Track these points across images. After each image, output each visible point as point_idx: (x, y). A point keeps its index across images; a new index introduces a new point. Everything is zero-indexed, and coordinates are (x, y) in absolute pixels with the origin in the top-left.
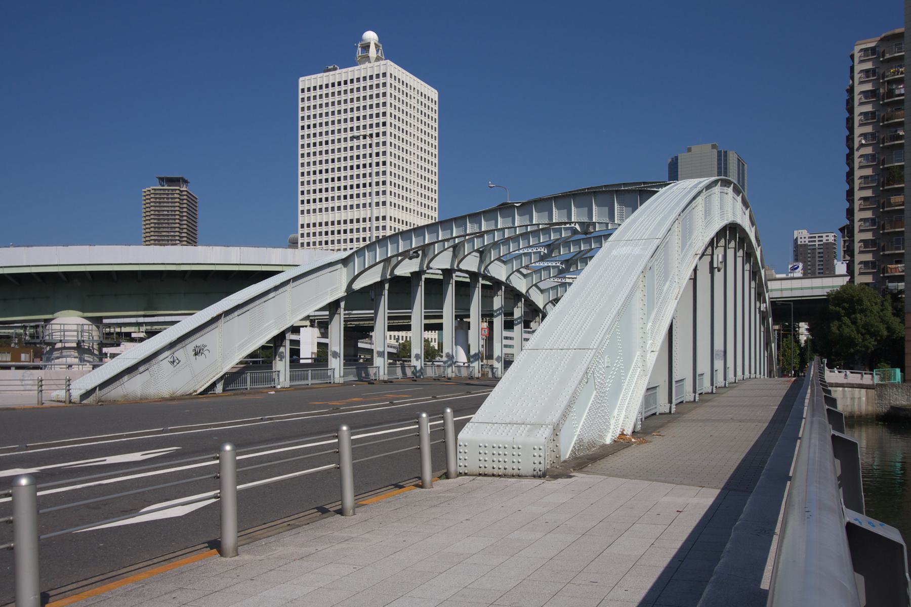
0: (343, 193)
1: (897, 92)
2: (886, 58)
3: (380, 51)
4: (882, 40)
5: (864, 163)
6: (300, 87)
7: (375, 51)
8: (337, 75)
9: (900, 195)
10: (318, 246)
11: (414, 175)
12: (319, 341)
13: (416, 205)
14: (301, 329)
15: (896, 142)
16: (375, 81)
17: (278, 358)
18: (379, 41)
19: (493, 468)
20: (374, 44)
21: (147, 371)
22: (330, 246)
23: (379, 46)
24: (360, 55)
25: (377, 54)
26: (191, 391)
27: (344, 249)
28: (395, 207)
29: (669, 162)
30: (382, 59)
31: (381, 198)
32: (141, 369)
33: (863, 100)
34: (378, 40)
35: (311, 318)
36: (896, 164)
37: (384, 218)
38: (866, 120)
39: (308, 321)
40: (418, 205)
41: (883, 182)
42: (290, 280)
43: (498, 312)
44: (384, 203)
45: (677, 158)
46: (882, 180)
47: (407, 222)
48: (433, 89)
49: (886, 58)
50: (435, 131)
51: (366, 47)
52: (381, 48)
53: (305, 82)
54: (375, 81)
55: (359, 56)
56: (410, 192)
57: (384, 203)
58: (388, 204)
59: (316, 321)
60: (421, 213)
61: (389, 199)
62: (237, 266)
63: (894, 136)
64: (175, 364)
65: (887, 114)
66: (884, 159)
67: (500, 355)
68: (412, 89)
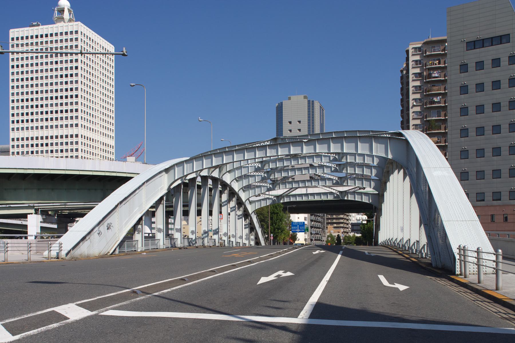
0: (45, 116)
1: (433, 75)
2: (427, 54)
3: (72, 15)
4: (424, 43)
5: (415, 117)
6: (11, 36)
7: (68, 14)
8: (40, 30)
9: (435, 137)
10: (45, 153)
11: (98, 106)
12: (41, 226)
13: (99, 127)
14: (28, 216)
15: (433, 105)
16: (69, 37)
17: (136, 232)
18: (71, 7)
19: (474, 271)
20: (67, 10)
21: (89, 239)
22: (55, 154)
23: (71, 11)
24: (57, 16)
25: (69, 16)
26: (107, 252)
27: (66, 156)
28: (85, 128)
29: (276, 106)
30: (73, 20)
31: (74, 122)
32: (87, 238)
33: (415, 78)
34: (70, 6)
35: (35, 208)
36: (433, 118)
37: (77, 136)
38: (416, 91)
39: (33, 210)
40: (101, 127)
41: (426, 128)
42: (145, 182)
43: (224, 204)
44: (77, 125)
45: (282, 103)
46: (425, 127)
47: (93, 139)
48: (111, 45)
49: (427, 54)
50: (113, 75)
51: (62, 11)
52: (72, 12)
53: (14, 33)
54: (69, 37)
55: (56, 17)
56: (95, 118)
57: (77, 125)
58: (80, 125)
59: (40, 210)
60: (103, 133)
61: (80, 122)
62: (16, 170)
63: (431, 101)
64: (100, 235)
65: (428, 88)
66: (426, 115)
67: (227, 232)
68: (97, 44)
